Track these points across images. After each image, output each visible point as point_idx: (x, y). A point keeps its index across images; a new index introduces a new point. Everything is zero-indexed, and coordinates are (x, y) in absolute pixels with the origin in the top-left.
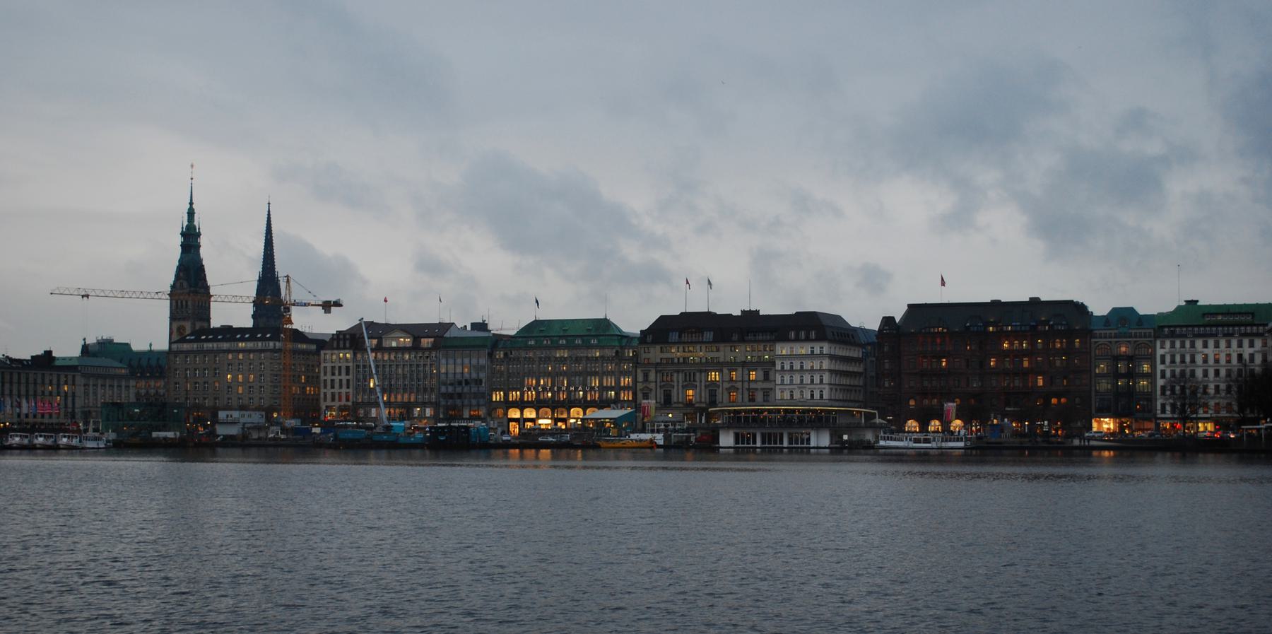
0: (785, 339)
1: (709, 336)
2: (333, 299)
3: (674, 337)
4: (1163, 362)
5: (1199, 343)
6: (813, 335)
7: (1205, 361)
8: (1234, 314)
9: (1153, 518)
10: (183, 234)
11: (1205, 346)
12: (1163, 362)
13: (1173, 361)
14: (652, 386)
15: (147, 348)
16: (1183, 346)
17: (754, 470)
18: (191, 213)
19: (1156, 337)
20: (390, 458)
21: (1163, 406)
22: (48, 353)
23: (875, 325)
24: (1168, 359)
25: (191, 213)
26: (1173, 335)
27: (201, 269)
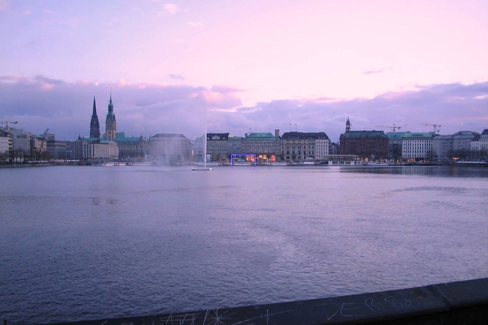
0: (318, 139)
1: (298, 137)
2: (47, 129)
3: (289, 138)
4: (404, 145)
5: (412, 141)
6: (324, 138)
7: (413, 145)
8: (419, 135)
9: (475, 187)
10: (109, 107)
11: (413, 142)
12: (404, 145)
13: (406, 145)
14: (284, 150)
15: (131, 137)
16: (408, 141)
17: (293, 172)
18: (111, 101)
19: (402, 140)
20: (432, 176)
21: (404, 155)
22: (383, 131)
23: (428, 132)
24: (405, 145)
25: (111, 101)
26: (405, 139)
27: (97, 117)
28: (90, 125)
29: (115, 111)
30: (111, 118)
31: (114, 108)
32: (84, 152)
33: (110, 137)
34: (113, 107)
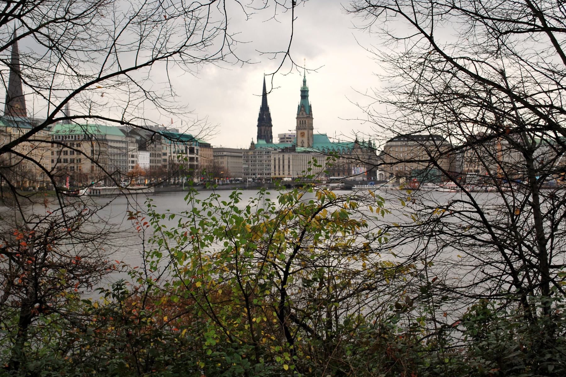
10: (302, 91)
18: (305, 82)
25: (305, 82)
28: (257, 123)
29: (312, 99)
30: (305, 113)
31: (310, 93)
32: (272, 167)
33: (303, 142)
34: (308, 91)
